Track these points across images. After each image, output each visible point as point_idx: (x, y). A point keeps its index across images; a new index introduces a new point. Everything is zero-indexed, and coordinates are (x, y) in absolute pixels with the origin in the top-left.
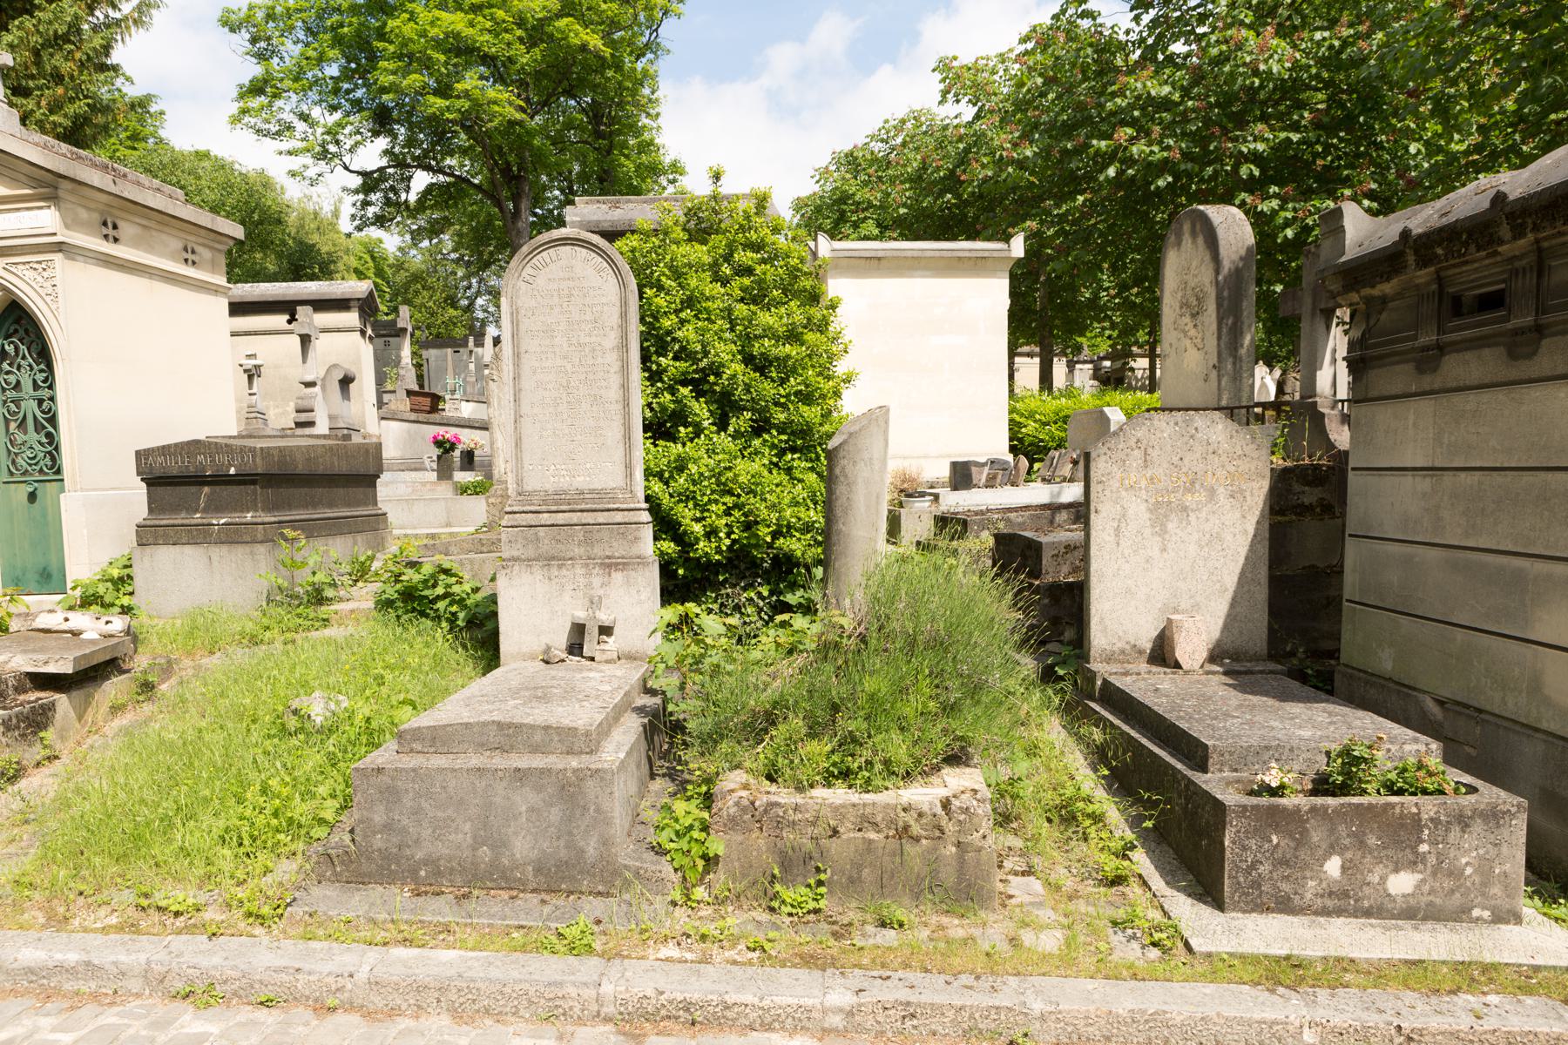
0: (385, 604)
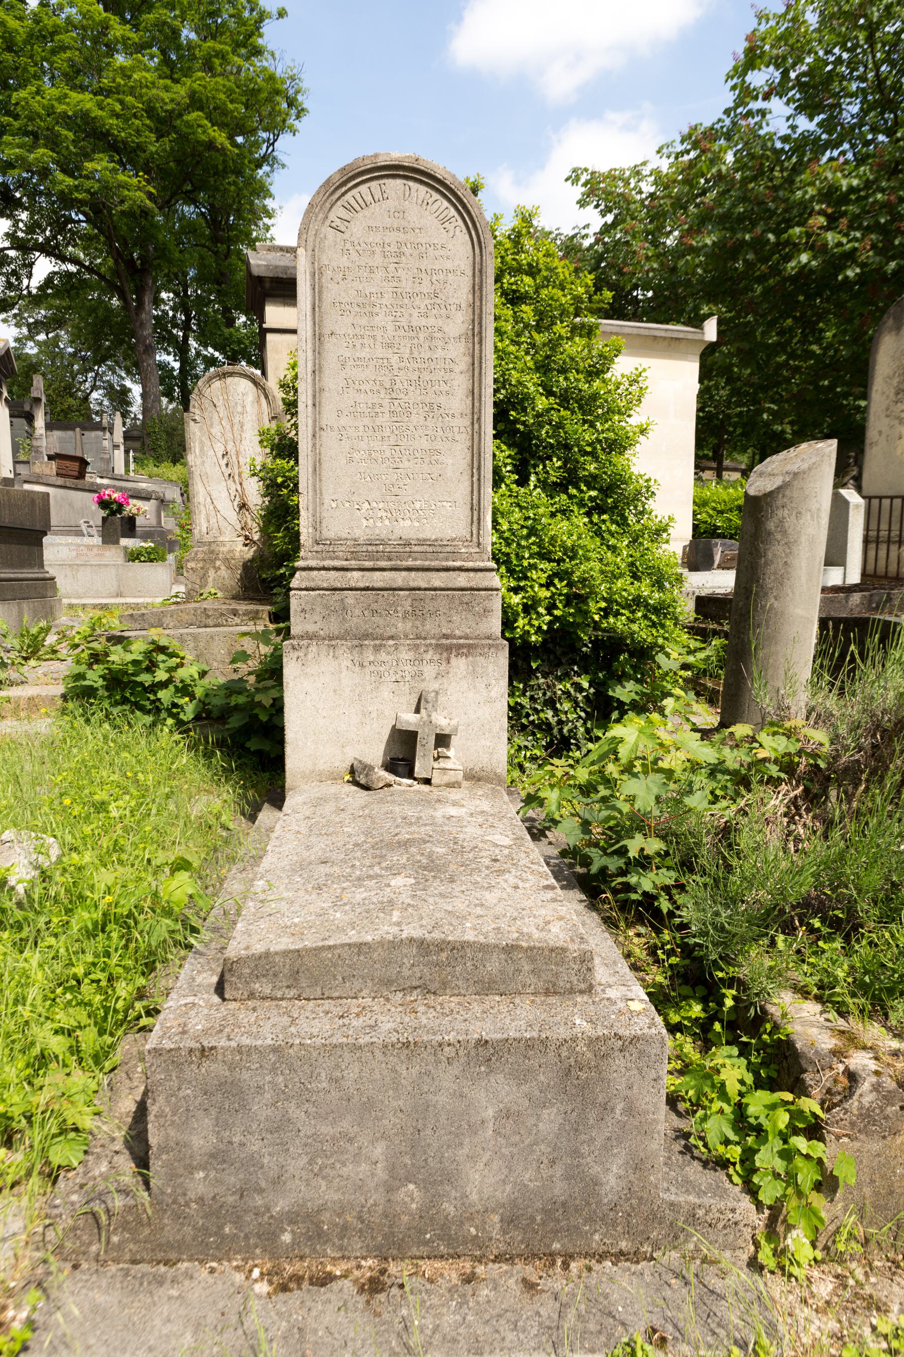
0: (81, 693)
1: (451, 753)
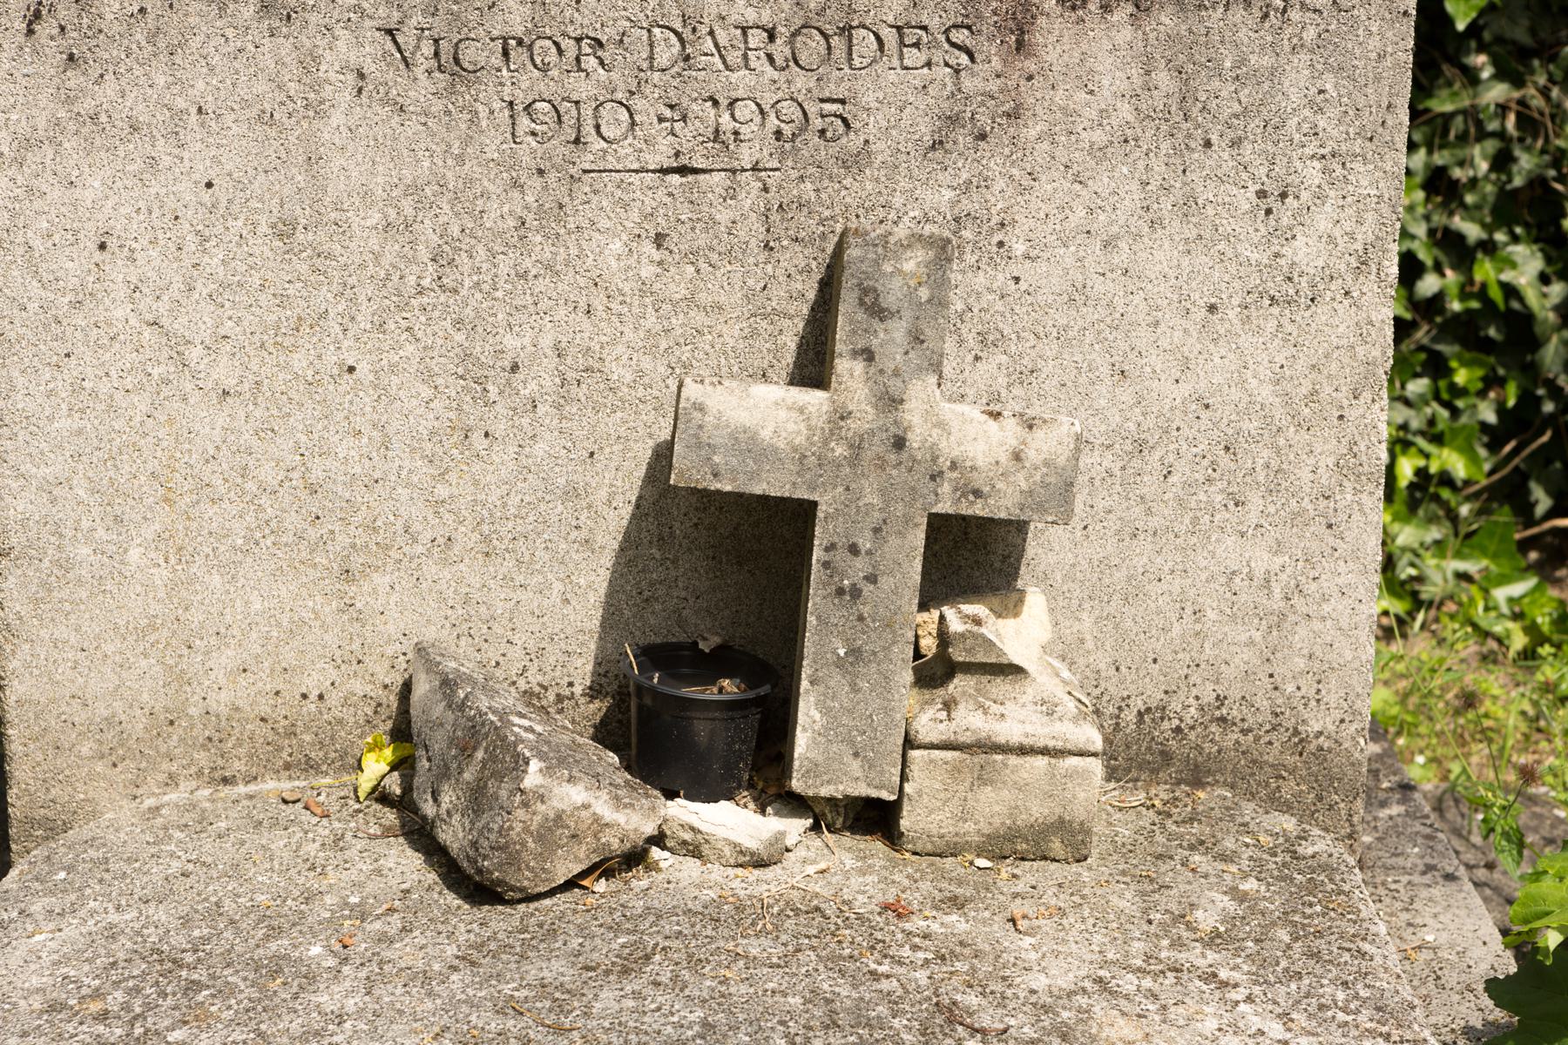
1: (1021, 633)
